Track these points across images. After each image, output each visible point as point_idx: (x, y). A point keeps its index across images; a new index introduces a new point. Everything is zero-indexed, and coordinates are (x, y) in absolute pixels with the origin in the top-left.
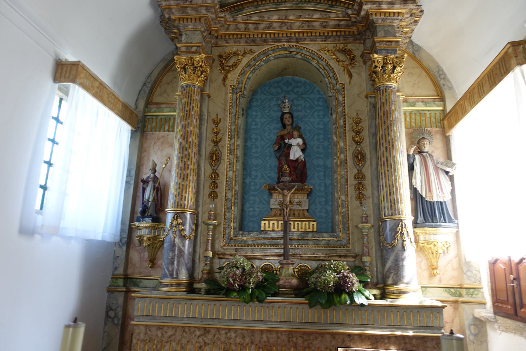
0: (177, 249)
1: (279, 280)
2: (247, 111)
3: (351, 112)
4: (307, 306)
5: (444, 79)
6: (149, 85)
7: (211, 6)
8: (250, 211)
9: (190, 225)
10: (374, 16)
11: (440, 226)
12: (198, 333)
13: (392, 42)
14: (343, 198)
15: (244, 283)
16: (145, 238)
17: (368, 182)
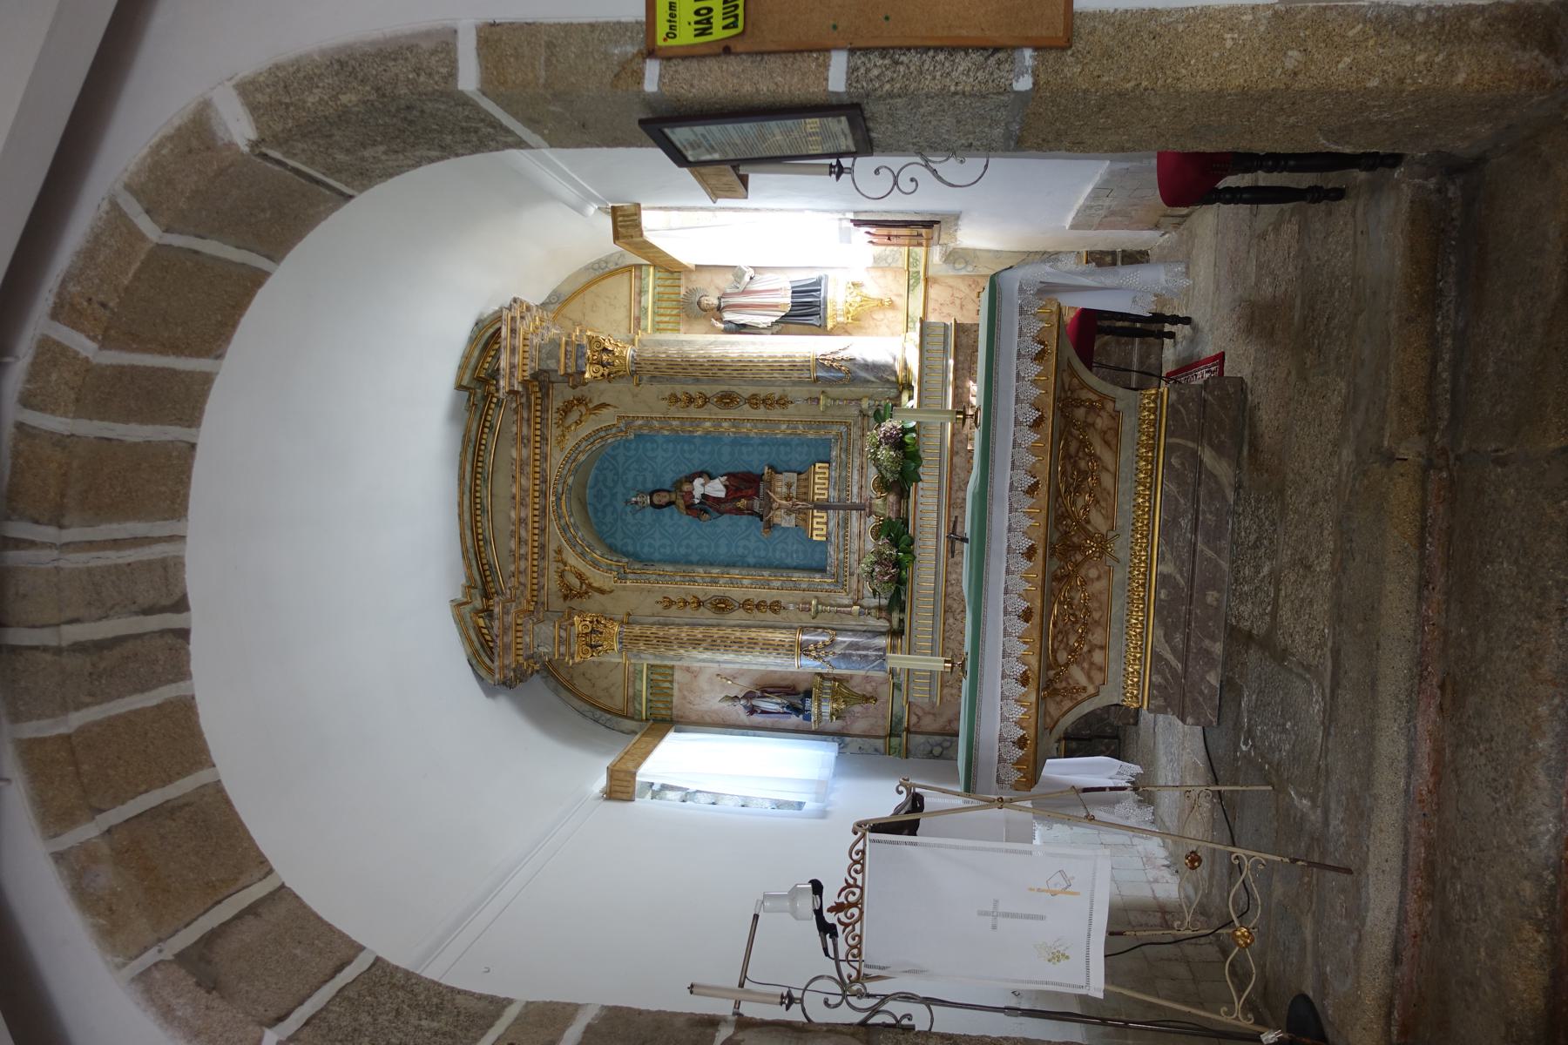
0: (847, 652)
1: (889, 518)
2: (647, 562)
3: (661, 408)
4: (920, 484)
5: (607, 263)
6: (598, 713)
7: (504, 607)
8: (798, 557)
9: (818, 635)
10: (525, 374)
11: (825, 298)
12: (951, 621)
13: (566, 351)
14: (784, 427)
15: (891, 561)
16: (834, 706)
17: (763, 392)
